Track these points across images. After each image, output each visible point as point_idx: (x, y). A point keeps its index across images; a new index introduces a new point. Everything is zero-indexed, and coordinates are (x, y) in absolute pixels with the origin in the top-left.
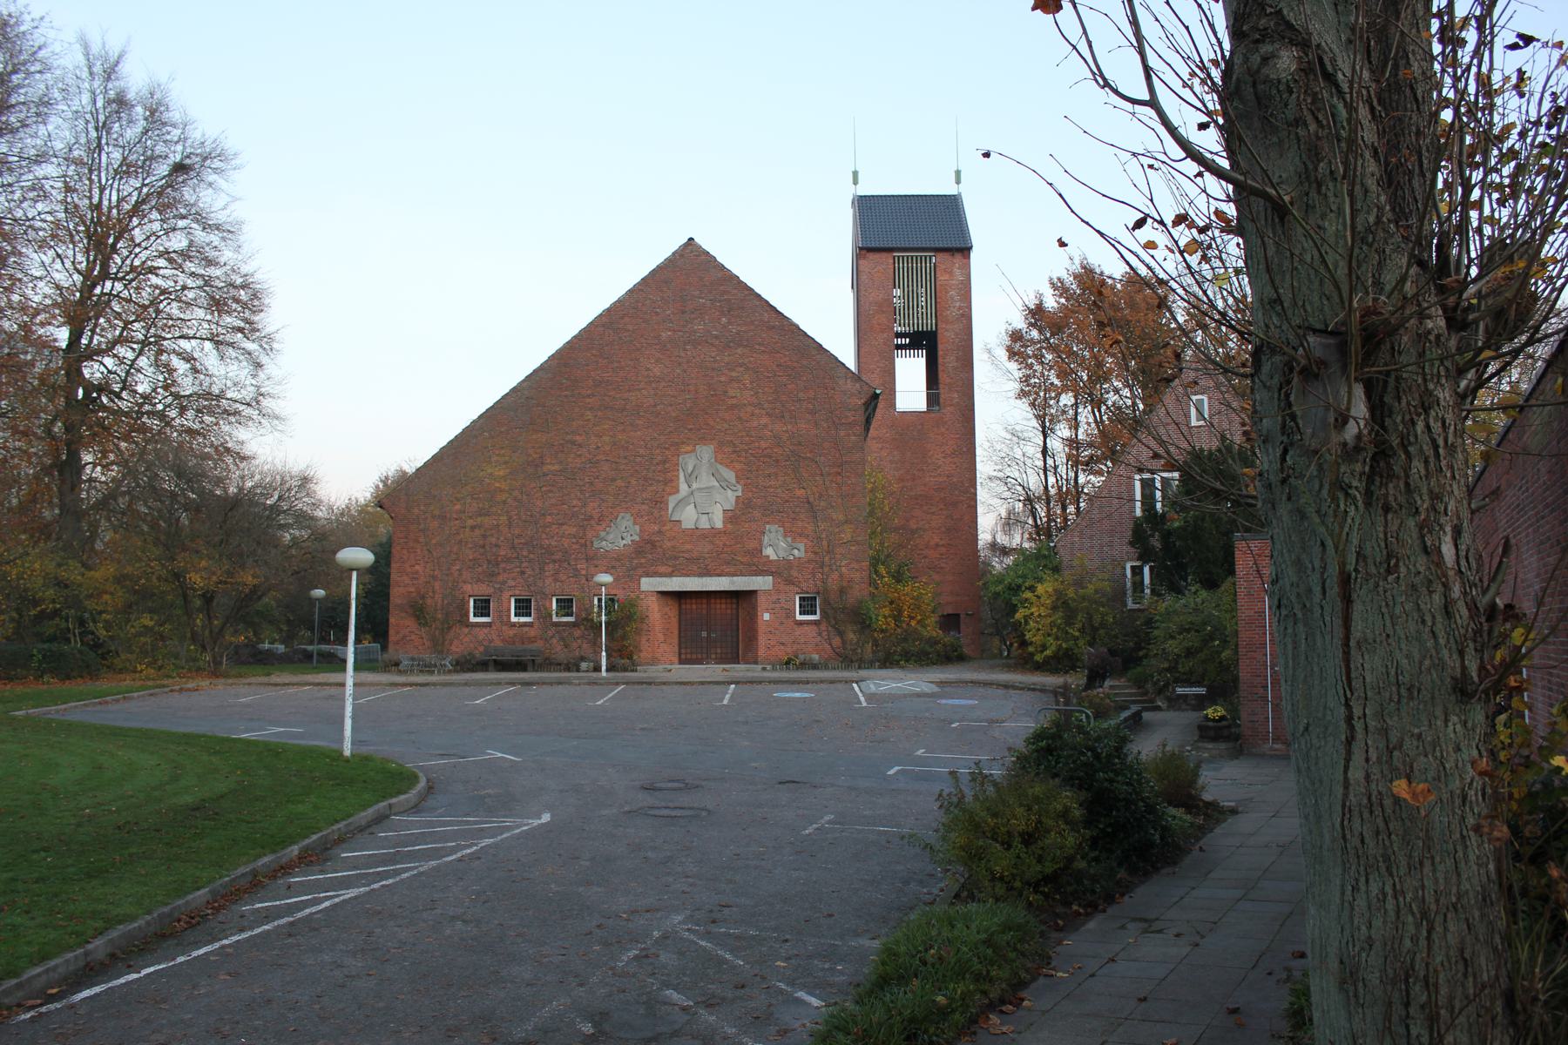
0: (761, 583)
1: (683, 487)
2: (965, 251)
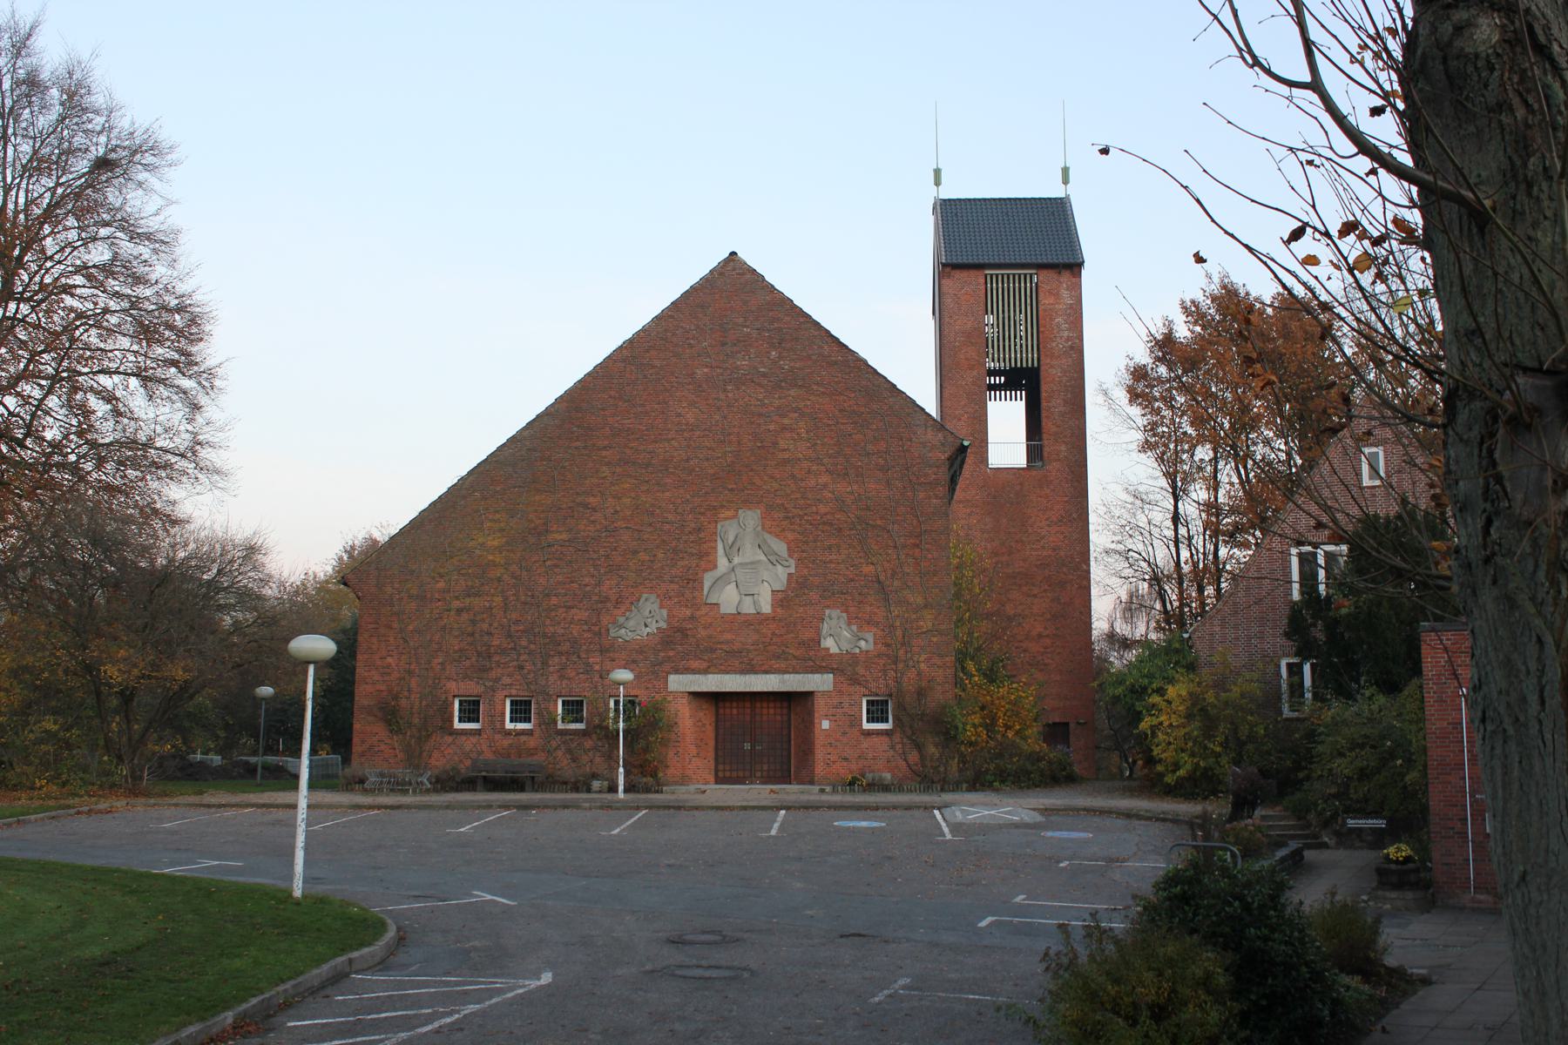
0: (819, 682)
1: (722, 562)
2: (1074, 267)
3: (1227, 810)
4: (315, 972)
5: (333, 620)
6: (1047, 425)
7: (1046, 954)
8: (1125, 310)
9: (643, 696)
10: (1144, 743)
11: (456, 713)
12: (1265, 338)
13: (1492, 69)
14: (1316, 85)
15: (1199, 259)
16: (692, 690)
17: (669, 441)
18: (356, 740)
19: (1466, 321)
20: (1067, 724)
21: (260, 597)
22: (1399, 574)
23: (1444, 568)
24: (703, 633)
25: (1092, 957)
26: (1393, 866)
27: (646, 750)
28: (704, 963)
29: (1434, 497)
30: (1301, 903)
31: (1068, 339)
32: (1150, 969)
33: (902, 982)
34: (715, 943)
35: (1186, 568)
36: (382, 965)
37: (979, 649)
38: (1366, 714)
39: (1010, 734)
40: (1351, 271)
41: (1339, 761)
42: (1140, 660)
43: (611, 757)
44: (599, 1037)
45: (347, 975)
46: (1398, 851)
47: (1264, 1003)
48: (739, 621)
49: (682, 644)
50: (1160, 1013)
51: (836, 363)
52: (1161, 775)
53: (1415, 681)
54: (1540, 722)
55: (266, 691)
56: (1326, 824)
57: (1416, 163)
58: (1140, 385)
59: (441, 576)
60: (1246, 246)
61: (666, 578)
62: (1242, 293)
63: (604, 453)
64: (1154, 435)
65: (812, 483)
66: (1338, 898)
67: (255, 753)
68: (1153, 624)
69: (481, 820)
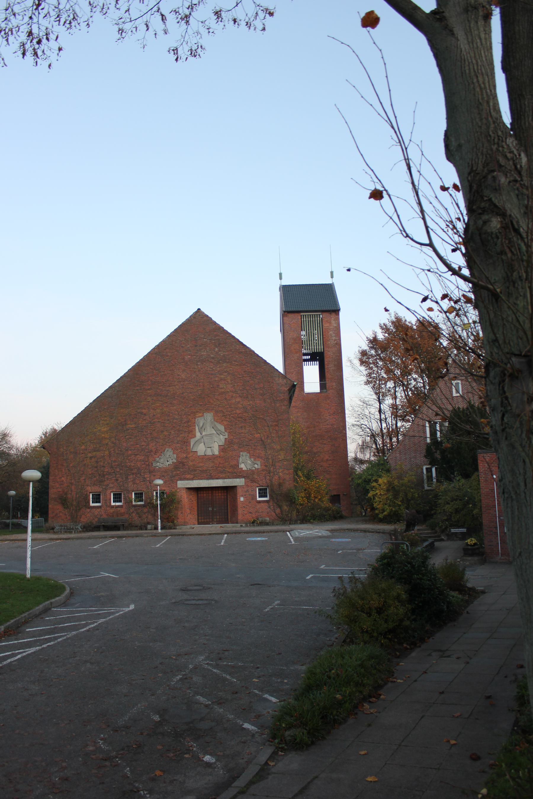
0: (239, 482)
1: (198, 435)
2: (336, 311)
3: (404, 527)
4: (37, 608)
5: (39, 463)
6: (328, 375)
7: (334, 590)
8: (357, 329)
9: (167, 490)
10: (370, 501)
11: (91, 500)
12: (412, 337)
13: (498, 238)
14: (431, 245)
15: (386, 310)
16: (187, 487)
17: (174, 386)
18: (50, 512)
19: (492, 336)
20: (339, 495)
21: (9, 454)
22: (469, 433)
23: (487, 430)
24: (191, 463)
25: (352, 590)
26: (469, 547)
27: (169, 512)
28: (196, 598)
29: (482, 403)
30: (434, 564)
31: (335, 340)
32: (376, 593)
33: (276, 603)
34: (200, 590)
35: (385, 431)
36: (64, 604)
37: (303, 466)
38: (458, 487)
39: (317, 500)
40: (445, 312)
41: (447, 506)
42: (368, 469)
43: (155, 515)
44: (154, 630)
45: (50, 609)
46: (471, 541)
47: (421, 604)
48: (205, 458)
49: (182, 469)
50: (380, 611)
51: (241, 352)
52: (377, 514)
53: (476, 473)
54: (525, 493)
55: (12, 493)
56: (443, 531)
57: (470, 274)
58: (364, 358)
59: (83, 444)
60: (406, 307)
61: (176, 441)
62: (403, 320)
63: (148, 391)
64: (370, 378)
65: (234, 401)
66: (449, 561)
67: (8, 518)
68: (372, 454)
69: (102, 543)
